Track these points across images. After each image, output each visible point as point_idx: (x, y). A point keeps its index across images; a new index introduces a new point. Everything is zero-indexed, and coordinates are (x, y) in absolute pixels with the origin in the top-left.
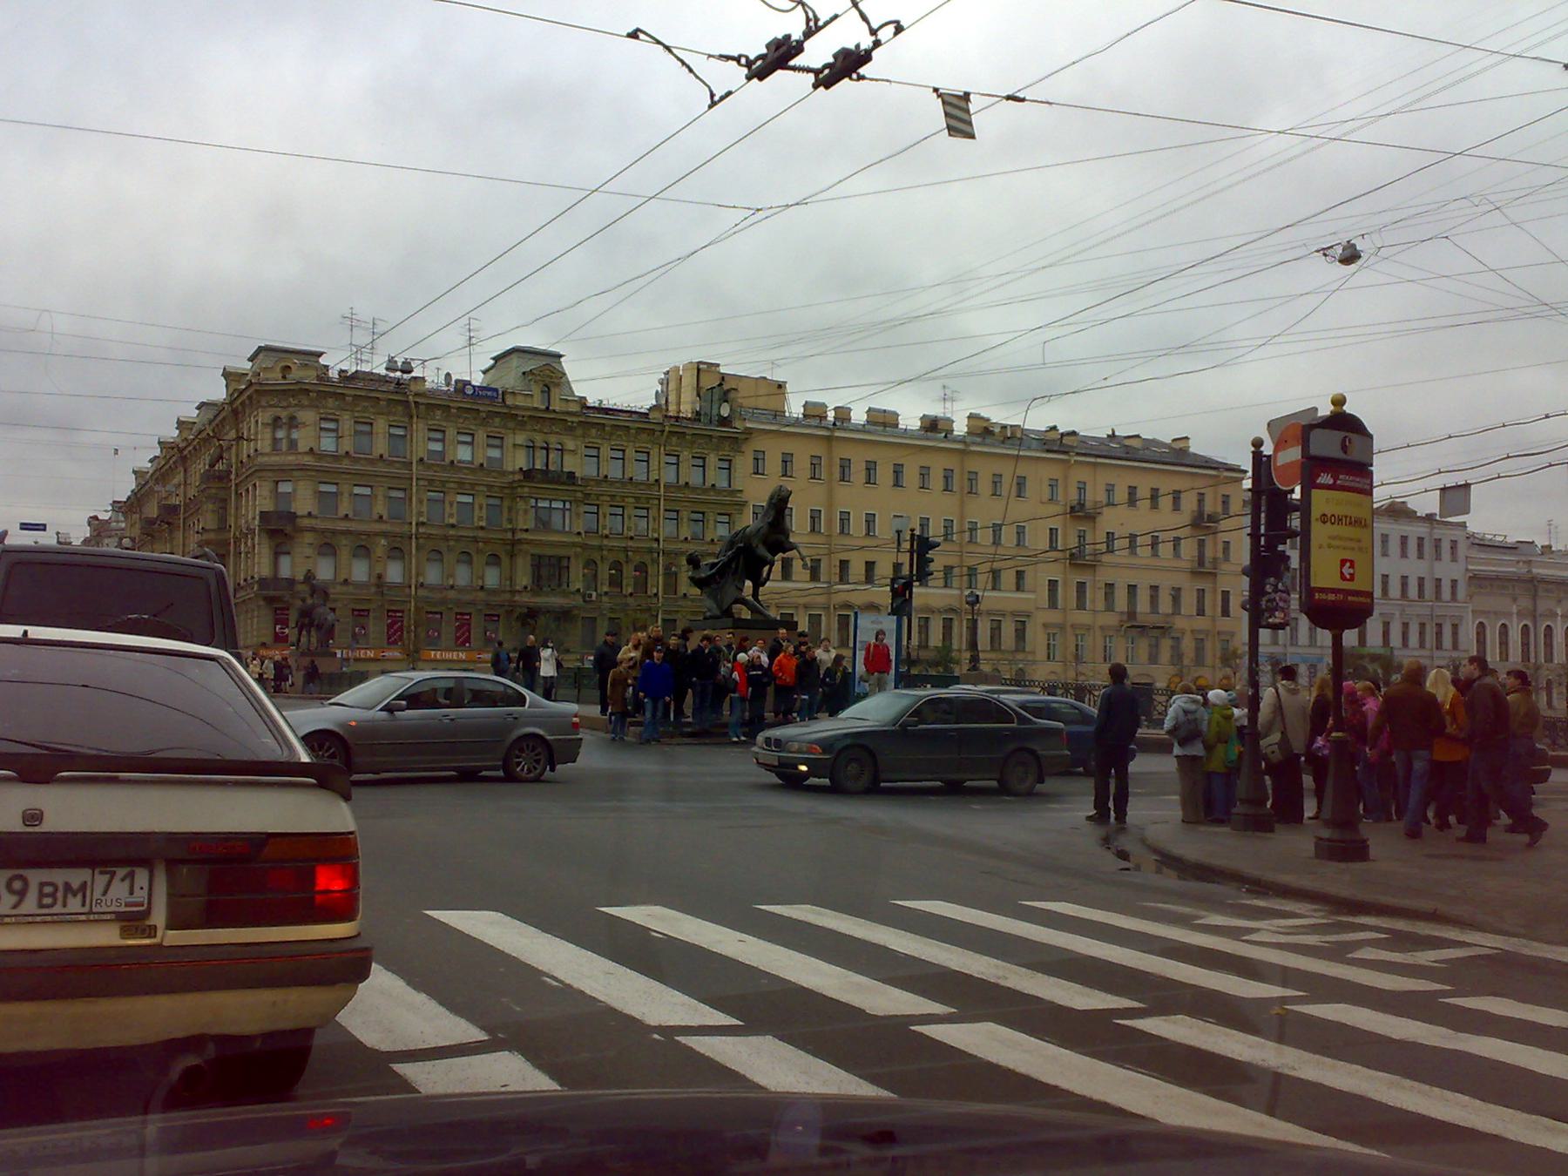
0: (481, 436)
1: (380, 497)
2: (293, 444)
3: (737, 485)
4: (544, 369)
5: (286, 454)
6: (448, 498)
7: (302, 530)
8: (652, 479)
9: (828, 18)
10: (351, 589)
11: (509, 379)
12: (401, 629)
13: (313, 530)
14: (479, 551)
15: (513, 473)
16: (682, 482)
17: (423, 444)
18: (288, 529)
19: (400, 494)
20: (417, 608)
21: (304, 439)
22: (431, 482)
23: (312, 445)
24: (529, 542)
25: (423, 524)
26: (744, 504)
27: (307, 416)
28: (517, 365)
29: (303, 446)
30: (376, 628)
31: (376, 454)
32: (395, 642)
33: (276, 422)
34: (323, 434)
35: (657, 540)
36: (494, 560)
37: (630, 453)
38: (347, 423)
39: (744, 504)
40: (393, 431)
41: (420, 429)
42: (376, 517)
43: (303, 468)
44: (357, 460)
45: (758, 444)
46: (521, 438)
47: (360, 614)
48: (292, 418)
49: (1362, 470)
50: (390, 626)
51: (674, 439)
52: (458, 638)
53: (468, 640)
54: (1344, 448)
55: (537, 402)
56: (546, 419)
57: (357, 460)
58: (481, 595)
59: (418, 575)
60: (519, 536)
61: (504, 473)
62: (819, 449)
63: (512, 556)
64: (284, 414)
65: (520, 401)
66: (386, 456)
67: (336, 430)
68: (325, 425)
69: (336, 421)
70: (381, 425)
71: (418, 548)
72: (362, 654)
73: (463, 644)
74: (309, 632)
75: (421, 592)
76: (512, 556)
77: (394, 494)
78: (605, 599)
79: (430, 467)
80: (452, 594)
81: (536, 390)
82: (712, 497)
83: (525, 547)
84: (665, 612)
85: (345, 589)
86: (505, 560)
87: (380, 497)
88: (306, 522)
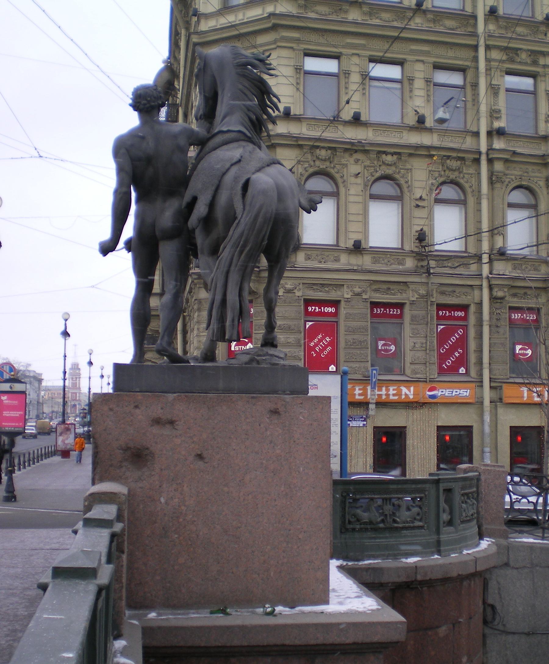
1: (419, 84)
9: (88, 390)
10: (366, 261)
12: (463, 342)
19: (456, 79)
25: (501, 132)
30: (415, 340)
32: (453, 369)
42: (411, 120)
44: (298, 119)
47: (386, 312)
49: (481, 260)
50: (442, 338)
52: (442, 358)
57: (298, 119)
71: (491, 182)
72: (391, 393)
75: (500, 267)
77: (442, 77)
79: (512, 22)
85: (355, 261)
87: (419, 84)
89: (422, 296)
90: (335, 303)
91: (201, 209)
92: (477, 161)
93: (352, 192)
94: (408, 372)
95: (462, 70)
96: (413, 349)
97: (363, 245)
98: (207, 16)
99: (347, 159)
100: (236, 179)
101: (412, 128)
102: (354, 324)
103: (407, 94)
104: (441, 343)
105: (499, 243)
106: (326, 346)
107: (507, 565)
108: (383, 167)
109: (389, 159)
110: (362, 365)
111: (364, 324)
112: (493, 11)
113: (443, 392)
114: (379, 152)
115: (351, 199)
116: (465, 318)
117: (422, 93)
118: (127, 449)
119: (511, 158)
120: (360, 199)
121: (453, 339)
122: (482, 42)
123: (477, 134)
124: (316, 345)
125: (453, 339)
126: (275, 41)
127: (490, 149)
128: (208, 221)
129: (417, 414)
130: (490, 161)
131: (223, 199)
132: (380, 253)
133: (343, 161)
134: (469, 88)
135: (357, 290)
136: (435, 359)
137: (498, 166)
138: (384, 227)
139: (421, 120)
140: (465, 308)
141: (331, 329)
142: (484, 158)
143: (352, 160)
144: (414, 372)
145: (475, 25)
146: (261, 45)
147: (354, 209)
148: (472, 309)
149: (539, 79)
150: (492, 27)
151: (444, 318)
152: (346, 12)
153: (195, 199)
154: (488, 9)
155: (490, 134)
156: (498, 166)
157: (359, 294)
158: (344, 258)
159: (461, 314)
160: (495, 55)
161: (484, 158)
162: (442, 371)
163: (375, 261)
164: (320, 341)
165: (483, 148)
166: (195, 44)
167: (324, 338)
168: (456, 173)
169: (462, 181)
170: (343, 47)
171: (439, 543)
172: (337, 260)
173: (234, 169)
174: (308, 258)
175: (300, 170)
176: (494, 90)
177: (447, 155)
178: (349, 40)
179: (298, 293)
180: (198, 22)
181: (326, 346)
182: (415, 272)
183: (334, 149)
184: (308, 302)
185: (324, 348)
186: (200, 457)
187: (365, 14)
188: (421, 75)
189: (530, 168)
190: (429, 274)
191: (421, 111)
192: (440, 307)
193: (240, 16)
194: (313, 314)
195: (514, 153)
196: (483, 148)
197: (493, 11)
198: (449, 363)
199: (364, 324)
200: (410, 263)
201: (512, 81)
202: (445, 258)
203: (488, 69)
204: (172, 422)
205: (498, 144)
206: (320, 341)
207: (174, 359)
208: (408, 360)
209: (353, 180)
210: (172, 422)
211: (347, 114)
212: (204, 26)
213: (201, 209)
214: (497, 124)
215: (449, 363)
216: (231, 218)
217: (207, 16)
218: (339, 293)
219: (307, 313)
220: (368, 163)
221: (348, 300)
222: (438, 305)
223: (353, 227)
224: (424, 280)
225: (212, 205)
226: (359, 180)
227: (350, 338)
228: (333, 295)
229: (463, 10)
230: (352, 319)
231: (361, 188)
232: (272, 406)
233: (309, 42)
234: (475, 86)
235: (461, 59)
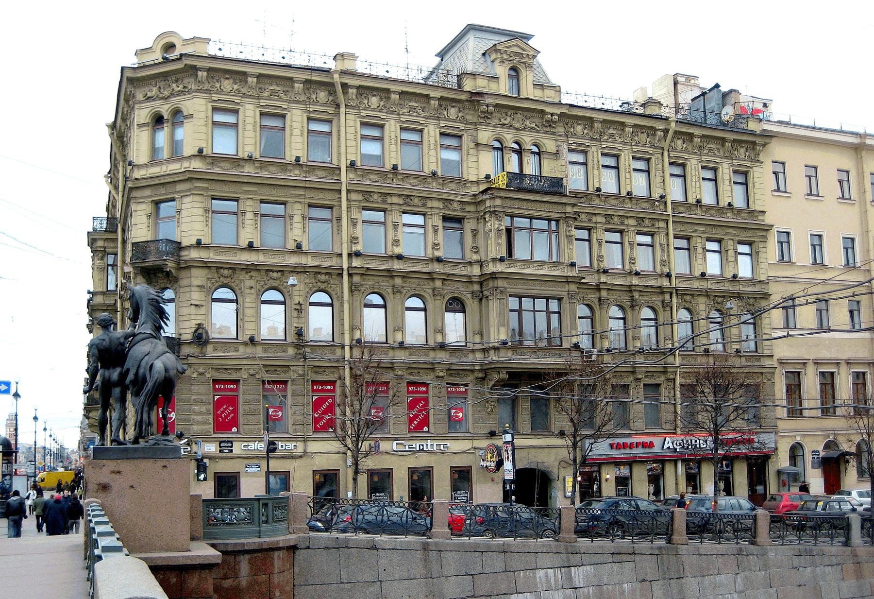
0: (432, 132)
2: (175, 145)
3: (756, 206)
4: (514, 50)
5: (169, 161)
6: (390, 219)
7: (188, 267)
8: (656, 195)
10: (259, 351)
11: (470, 57)
13: (206, 265)
14: (435, 292)
15: (477, 182)
16: (692, 200)
17: (352, 143)
18: (170, 265)
20: (354, 377)
21: (190, 136)
22: (367, 194)
23: (202, 144)
24: (507, 277)
25: (358, 254)
26: (768, 228)
27: (196, 106)
28: (474, 46)
29: (189, 150)
30: (296, 407)
31: (290, 158)
33: (158, 120)
34: (218, 132)
35: (669, 276)
36: (456, 304)
37: (626, 159)
38: (249, 112)
39: (768, 228)
40: (314, 127)
41: (349, 123)
42: (291, 246)
43: (191, 177)
44: (207, 247)
45: (778, 151)
46: (485, 135)
48: (177, 112)
50: (316, 405)
51: (679, 143)
52: (411, 420)
53: (425, 422)
54: (140, 126)
55: (504, 87)
56: (512, 109)
57: (207, 247)
58: (442, 356)
59: (352, 329)
60: (491, 268)
61: (461, 182)
62: (846, 162)
63: (481, 298)
64: (165, 110)
65: (481, 85)
66: (303, 160)
69: (236, 112)
70: (296, 117)
71: (351, 291)
73: (419, 428)
74: (123, 400)
76: (481, 298)
78: (607, 358)
79: (366, 172)
80: (401, 356)
81: (502, 71)
82: (729, 217)
83: (500, 283)
84: (684, 375)
85: (250, 350)
86: (471, 305)
88: (194, 254)
89: (300, 376)
90: (236, 382)
91: (131, 376)
92: (341, 275)
93: (247, 300)
94: (290, 431)
95: (331, 207)
96: (294, 414)
97: (256, 339)
98: (139, 166)
99: (243, 276)
100: (147, 363)
101: (292, 252)
102: (248, 397)
103: (288, 226)
104: (315, 410)
105: (357, 335)
106: (230, 414)
107: (308, 548)
108: (271, 281)
109: (275, 275)
110: (256, 427)
111: (257, 397)
112: (352, 164)
113: (313, 447)
114: (268, 270)
115: (247, 305)
116: (333, 391)
117: (300, 225)
118: (99, 484)
119: (366, 273)
120: (254, 305)
121: (325, 406)
122: (344, 189)
123: (341, 255)
124: (222, 412)
125: (325, 406)
126: (190, 190)
127: (350, 267)
128: (135, 382)
129: (298, 462)
130: (350, 275)
131: (141, 371)
132: (268, 345)
133: (241, 277)
134: (335, 221)
135: (252, 372)
136: (310, 420)
137: (356, 279)
138: (272, 321)
139: (299, 246)
140: (333, 383)
141: (233, 401)
142: (345, 273)
143: (247, 276)
144: (295, 431)
145: (340, 174)
146: (179, 192)
147: (248, 312)
148: (338, 384)
149: (387, 213)
150: (351, 176)
151: (413, 392)
152: (243, 167)
153: (128, 370)
154: (349, 162)
155: (350, 255)
156: (356, 279)
157: (252, 375)
158: (242, 348)
159: (233, 387)
160: (354, 196)
161: (345, 273)
162: (316, 430)
163: (265, 351)
164: (225, 409)
165: (345, 267)
166: (131, 189)
167: (228, 407)
168: (326, 284)
169: (330, 290)
170: (240, 193)
171: (260, 532)
172: (237, 350)
173: (146, 358)
174: (215, 349)
175: (209, 285)
176: (354, 223)
177: (317, 271)
179: (208, 376)
180: (132, 170)
181: (230, 414)
182: (295, 357)
183: (234, 269)
184: (216, 381)
185: (228, 415)
186: (132, 487)
187: (257, 168)
188: (299, 212)
189: (381, 279)
190: (305, 359)
191: (299, 239)
192: (314, 382)
193: (164, 168)
194: (220, 390)
195: (368, 268)
196: (345, 267)
197: (352, 164)
198: (321, 423)
199: (257, 397)
200: (291, 351)
201: (368, 215)
202: (318, 347)
203: (349, 208)
204: (119, 472)
205: (356, 263)
206: (225, 409)
207: (120, 443)
208: (290, 423)
209: (248, 291)
210: (119, 472)
211: (244, 243)
212: (138, 174)
213: (131, 376)
214: (355, 248)
215: (321, 423)
216: (144, 380)
217: (139, 166)
218: (238, 374)
219: (215, 390)
220: (259, 279)
221: (245, 380)
222: (313, 381)
223: (248, 326)
224: (301, 364)
225: (136, 374)
226: (253, 291)
227: (247, 407)
228: (234, 376)
229: (331, 163)
230: (248, 395)
231: (254, 296)
232: (164, 464)
233: (215, 190)
234: (339, 219)
235: (329, 200)
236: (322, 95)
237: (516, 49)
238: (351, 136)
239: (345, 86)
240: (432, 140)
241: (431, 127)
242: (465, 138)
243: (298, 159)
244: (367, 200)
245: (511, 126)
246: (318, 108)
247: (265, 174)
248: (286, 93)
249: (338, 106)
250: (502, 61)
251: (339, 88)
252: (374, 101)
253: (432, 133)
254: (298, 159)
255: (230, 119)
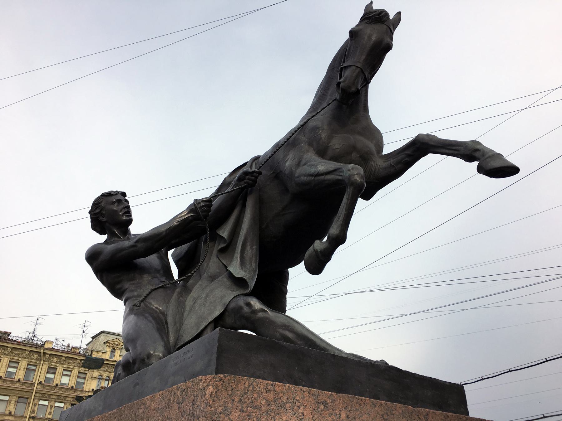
15: (89, 392)
42: (7, 412)
67: (35, 370)
68: (65, 373)
155: (30, 417)
160: (37, 395)
178: (14, 392)
236: (36, 356)
237: (116, 343)
238: (43, 372)
239: (45, 354)
240: (75, 375)
241: (76, 370)
242: (88, 375)
243: (19, 379)
244: (58, 399)
245: (107, 371)
246: (33, 361)
247: (5, 384)
248: (22, 354)
249: (41, 360)
250: (109, 347)
251: (42, 354)
252: (55, 359)
253: (75, 372)
254: (19, 379)
255: (68, 373)
